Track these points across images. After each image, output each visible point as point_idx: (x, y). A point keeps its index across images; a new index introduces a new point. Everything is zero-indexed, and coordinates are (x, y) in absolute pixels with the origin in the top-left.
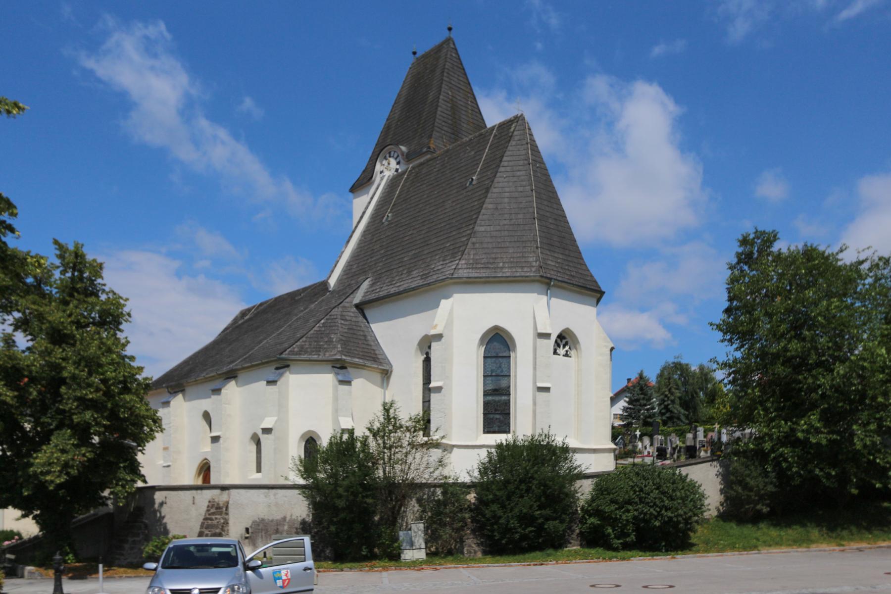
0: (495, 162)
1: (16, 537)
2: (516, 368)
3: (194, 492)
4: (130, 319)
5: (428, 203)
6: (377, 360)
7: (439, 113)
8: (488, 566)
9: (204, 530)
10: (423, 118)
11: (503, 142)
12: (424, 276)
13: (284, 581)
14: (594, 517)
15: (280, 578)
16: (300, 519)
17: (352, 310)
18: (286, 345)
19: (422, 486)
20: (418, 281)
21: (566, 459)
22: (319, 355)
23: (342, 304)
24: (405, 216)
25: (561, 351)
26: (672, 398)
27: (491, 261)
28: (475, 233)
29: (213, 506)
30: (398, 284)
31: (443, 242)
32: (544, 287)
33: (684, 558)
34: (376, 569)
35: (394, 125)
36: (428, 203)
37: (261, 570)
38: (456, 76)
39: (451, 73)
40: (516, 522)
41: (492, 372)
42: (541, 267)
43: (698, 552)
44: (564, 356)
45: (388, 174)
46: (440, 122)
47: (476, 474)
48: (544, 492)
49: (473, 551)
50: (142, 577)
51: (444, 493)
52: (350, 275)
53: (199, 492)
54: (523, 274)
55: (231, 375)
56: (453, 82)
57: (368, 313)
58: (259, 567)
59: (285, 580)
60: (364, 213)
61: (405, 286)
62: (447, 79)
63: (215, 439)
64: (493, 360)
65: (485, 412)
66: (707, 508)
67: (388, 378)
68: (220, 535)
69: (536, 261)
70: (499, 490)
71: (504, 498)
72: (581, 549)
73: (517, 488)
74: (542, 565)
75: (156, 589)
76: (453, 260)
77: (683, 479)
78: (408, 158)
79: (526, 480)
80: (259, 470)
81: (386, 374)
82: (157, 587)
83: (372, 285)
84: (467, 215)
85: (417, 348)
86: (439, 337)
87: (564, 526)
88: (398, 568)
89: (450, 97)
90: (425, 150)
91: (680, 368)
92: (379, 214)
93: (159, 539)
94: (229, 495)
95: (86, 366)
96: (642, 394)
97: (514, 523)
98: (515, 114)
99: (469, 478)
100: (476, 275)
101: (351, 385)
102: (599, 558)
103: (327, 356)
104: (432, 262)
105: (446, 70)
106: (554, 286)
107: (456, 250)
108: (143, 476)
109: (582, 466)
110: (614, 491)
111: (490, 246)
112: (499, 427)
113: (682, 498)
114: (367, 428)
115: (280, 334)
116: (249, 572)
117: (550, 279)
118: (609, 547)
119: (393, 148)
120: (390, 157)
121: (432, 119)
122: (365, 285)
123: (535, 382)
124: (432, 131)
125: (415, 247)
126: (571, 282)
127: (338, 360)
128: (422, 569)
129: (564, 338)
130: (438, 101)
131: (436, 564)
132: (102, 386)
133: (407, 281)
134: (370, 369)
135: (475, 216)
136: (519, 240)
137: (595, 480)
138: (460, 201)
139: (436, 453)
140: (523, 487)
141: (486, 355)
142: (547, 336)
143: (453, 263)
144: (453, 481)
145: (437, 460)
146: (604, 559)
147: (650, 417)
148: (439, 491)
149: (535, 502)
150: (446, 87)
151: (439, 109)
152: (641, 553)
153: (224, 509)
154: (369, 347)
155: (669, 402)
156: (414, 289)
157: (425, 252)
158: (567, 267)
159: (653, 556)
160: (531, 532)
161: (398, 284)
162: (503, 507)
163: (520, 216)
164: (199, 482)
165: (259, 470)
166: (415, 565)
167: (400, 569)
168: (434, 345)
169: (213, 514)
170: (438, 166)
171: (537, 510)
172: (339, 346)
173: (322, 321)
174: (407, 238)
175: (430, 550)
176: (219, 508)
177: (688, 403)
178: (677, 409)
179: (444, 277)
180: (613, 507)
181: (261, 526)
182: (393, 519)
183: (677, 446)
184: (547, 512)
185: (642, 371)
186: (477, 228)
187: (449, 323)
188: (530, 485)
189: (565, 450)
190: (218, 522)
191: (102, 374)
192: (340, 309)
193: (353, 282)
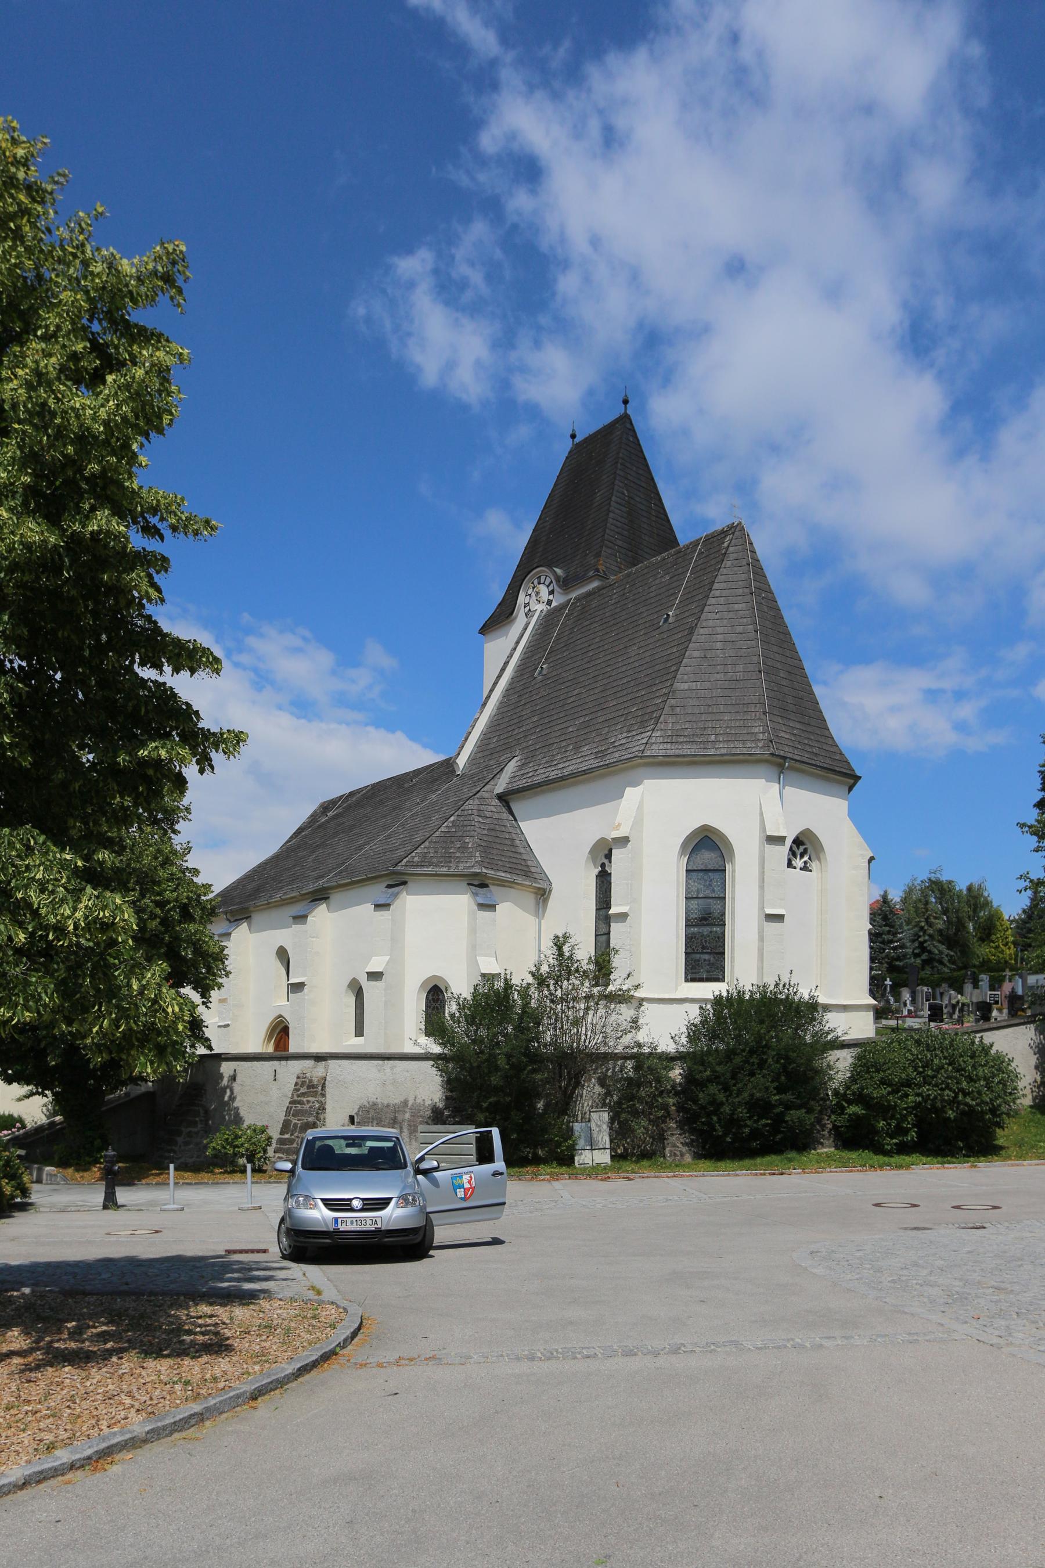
0: (702, 591)
1: (18, 1125)
2: (733, 886)
3: (276, 1063)
4: (189, 817)
5: (601, 649)
6: (529, 874)
7: (610, 520)
8: (704, 1176)
9: (290, 1118)
10: (588, 528)
11: (713, 562)
12: (600, 754)
13: (466, 1190)
14: (857, 1105)
15: (461, 1186)
16: (428, 1102)
17: (493, 803)
18: (401, 853)
19: (606, 1057)
20: (592, 761)
21: (814, 1019)
22: (450, 867)
23: (480, 794)
24: (568, 668)
25: (799, 863)
26: (931, 931)
27: (698, 732)
28: (674, 692)
29: (303, 1083)
30: (561, 766)
31: (626, 705)
32: (773, 771)
33: (989, 1167)
34: (542, 1177)
35: (544, 538)
36: (601, 649)
37: (436, 1174)
38: (634, 469)
39: (628, 465)
40: (745, 1111)
41: (698, 893)
42: (771, 741)
43: (1009, 1158)
44: (801, 869)
45: (539, 608)
46: (612, 534)
47: (684, 1040)
48: (784, 1067)
49: (678, 1153)
50: (207, 1183)
51: (637, 1068)
52: (486, 753)
53: (283, 1063)
54: (745, 751)
55: (320, 896)
56: (629, 477)
57: (514, 807)
58: (436, 1169)
59: (468, 1189)
60: (506, 663)
61: (571, 768)
62: (621, 473)
63: (297, 987)
64: (701, 875)
65: (688, 950)
66: (1021, 1093)
67: (546, 901)
68: (314, 1126)
69: (763, 733)
70: (720, 1064)
71: (728, 1075)
72: (836, 1152)
73: (746, 1062)
74: (782, 1174)
75: (301, 1199)
76: (643, 730)
77: (986, 1050)
78: (566, 584)
79: (759, 1048)
80: (359, 1031)
81: (543, 895)
82: (302, 1196)
83: (520, 767)
84: (662, 666)
85: (588, 857)
86: (624, 841)
87: (812, 1118)
88: (574, 1176)
89: (627, 498)
90: (591, 573)
91: (940, 888)
92: (528, 665)
93: (230, 1130)
94: (326, 1068)
95: (137, 883)
96: (885, 925)
97: (742, 1112)
98: (729, 522)
99: (674, 1046)
100: (678, 752)
101: (495, 911)
102: (865, 1166)
103: (461, 868)
104: (611, 734)
105: (620, 461)
106: (790, 768)
107: (647, 717)
108: (208, 1039)
109: (838, 1030)
110: (885, 1067)
111: (696, 710)
112: (708, 972)
113: (985, 1079)
114: (530, 972)
115: (389, 836)
116: (420, 1177)
117: (785, 758)
118: (879, 1150)
119: (544, 571)
120: (539, 583)
121: (600, 530)
122: (511, 767)
123: (762, 907)
124: (602, 547)
125: (584, 713)
126: (814, 763)
127: (476, 874)
128: (609, 1178)
129: (802, 843)
130: (609, 504)
131: (628, 1172)
132: (158, 911)
133: (574, 762)
134: (520, 887)
135: (674, 668)
136: (738, 702)
137: (854, 1051)
138: (651, 647)
139: (625, 1013)
140: (754, 1060)
141: (690, 868)
142: (779, 840)
143: (643, 735)
144: (649, 1050)
145: (629, 1019)
146: (872, 1166)
147: (898, 959)
148: (629, 1064)
149: (772, 1081)
150: (621, 484)
151: (611, 515)
152: (924, 1159)
153: (320, 1088)
154: (518, 856)
155: (927, 938)
156: (585, 772)
157: (601, 720)
158: (806, 742)
159: (943, 1163)
160: (767, 1125)
161: (561, 766)
162: (726, 1088)
163: (740, 668)
164: (270, 1049)
165: (359, 1031)
166: (595, 1172)
167: (576, 1178)
168: (616, 853)
169: (304, 1094)
170: (615, 596)
171: (774, 1095)
172: (477, 854)
173: (452, 819)
174: (572, 700)
175: (616, 1152)
176: (311, 1086)
177: (954, 939)
178: (939, 948)
179: (630, 756)
180: (885, 1090)
181: (372, 1113)
182: (565, 1105)
183: (958, 1002)
184: (789, 1097)
185: (886, 892)
186: (678, 686)
187: (638, 821)
188: (765, 1057)
189: (813, 1007)
190: (311, 1107)
191: (159, 894)
192: (477, 802)
193: (492, 762)
